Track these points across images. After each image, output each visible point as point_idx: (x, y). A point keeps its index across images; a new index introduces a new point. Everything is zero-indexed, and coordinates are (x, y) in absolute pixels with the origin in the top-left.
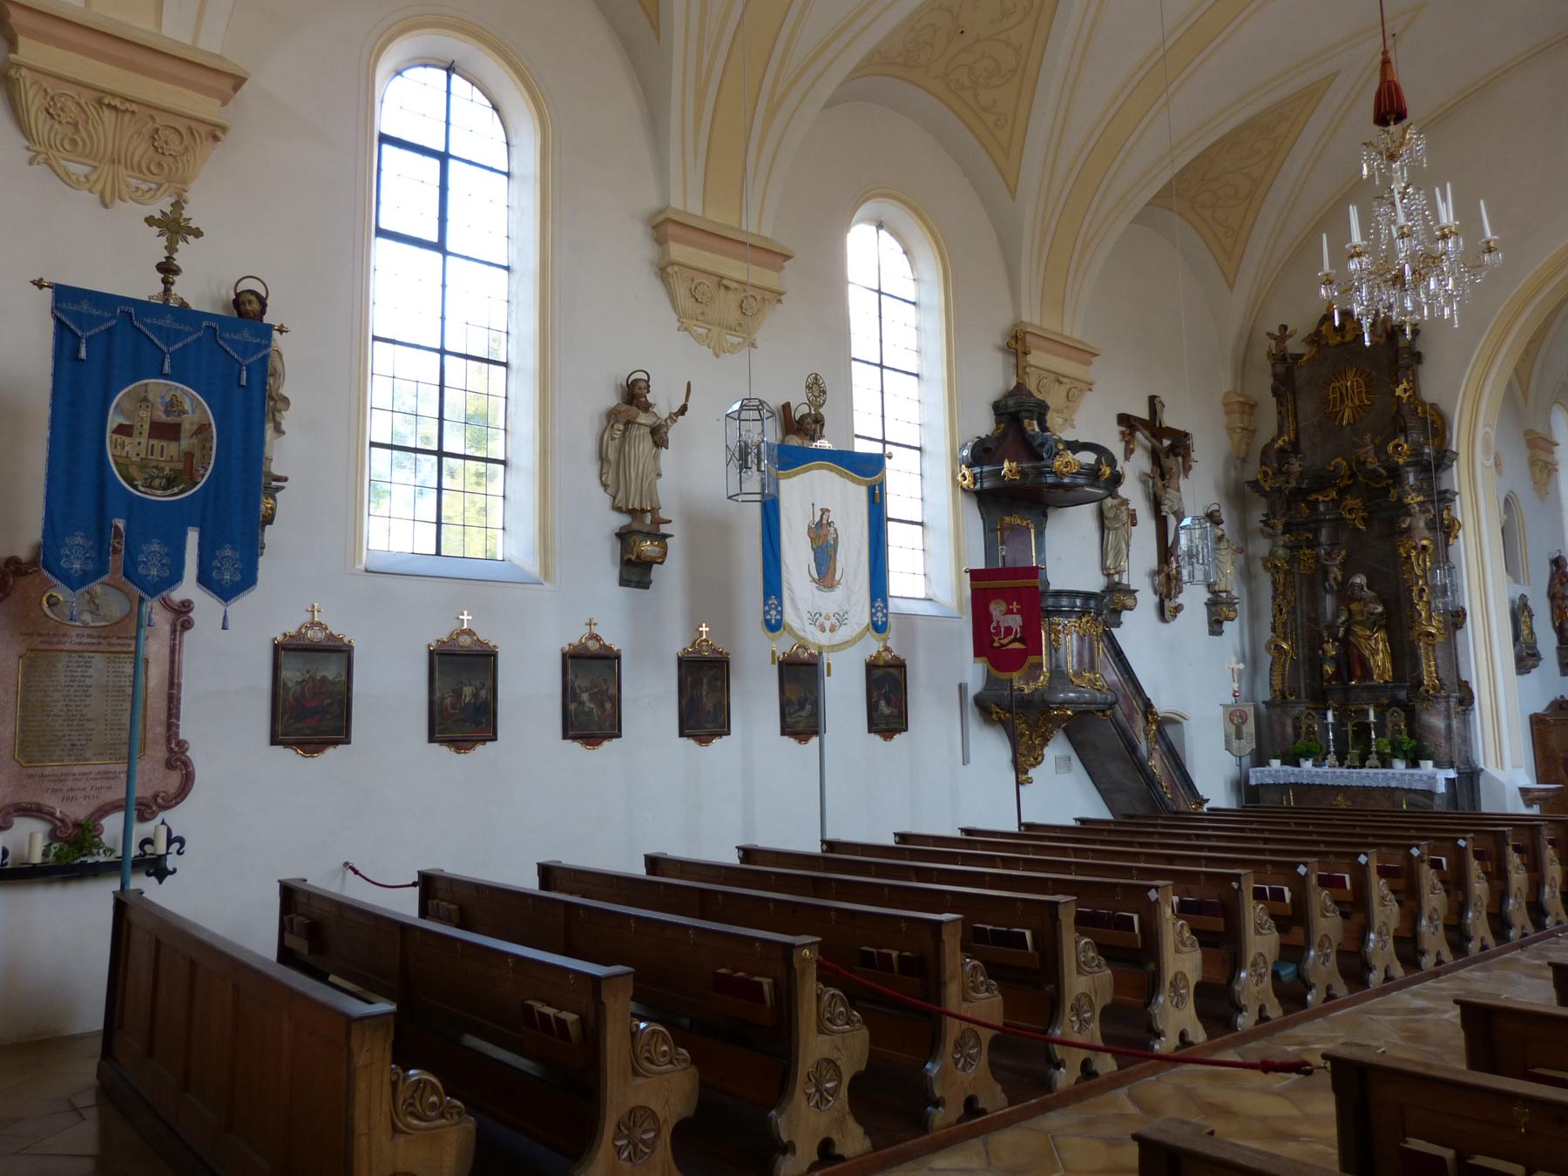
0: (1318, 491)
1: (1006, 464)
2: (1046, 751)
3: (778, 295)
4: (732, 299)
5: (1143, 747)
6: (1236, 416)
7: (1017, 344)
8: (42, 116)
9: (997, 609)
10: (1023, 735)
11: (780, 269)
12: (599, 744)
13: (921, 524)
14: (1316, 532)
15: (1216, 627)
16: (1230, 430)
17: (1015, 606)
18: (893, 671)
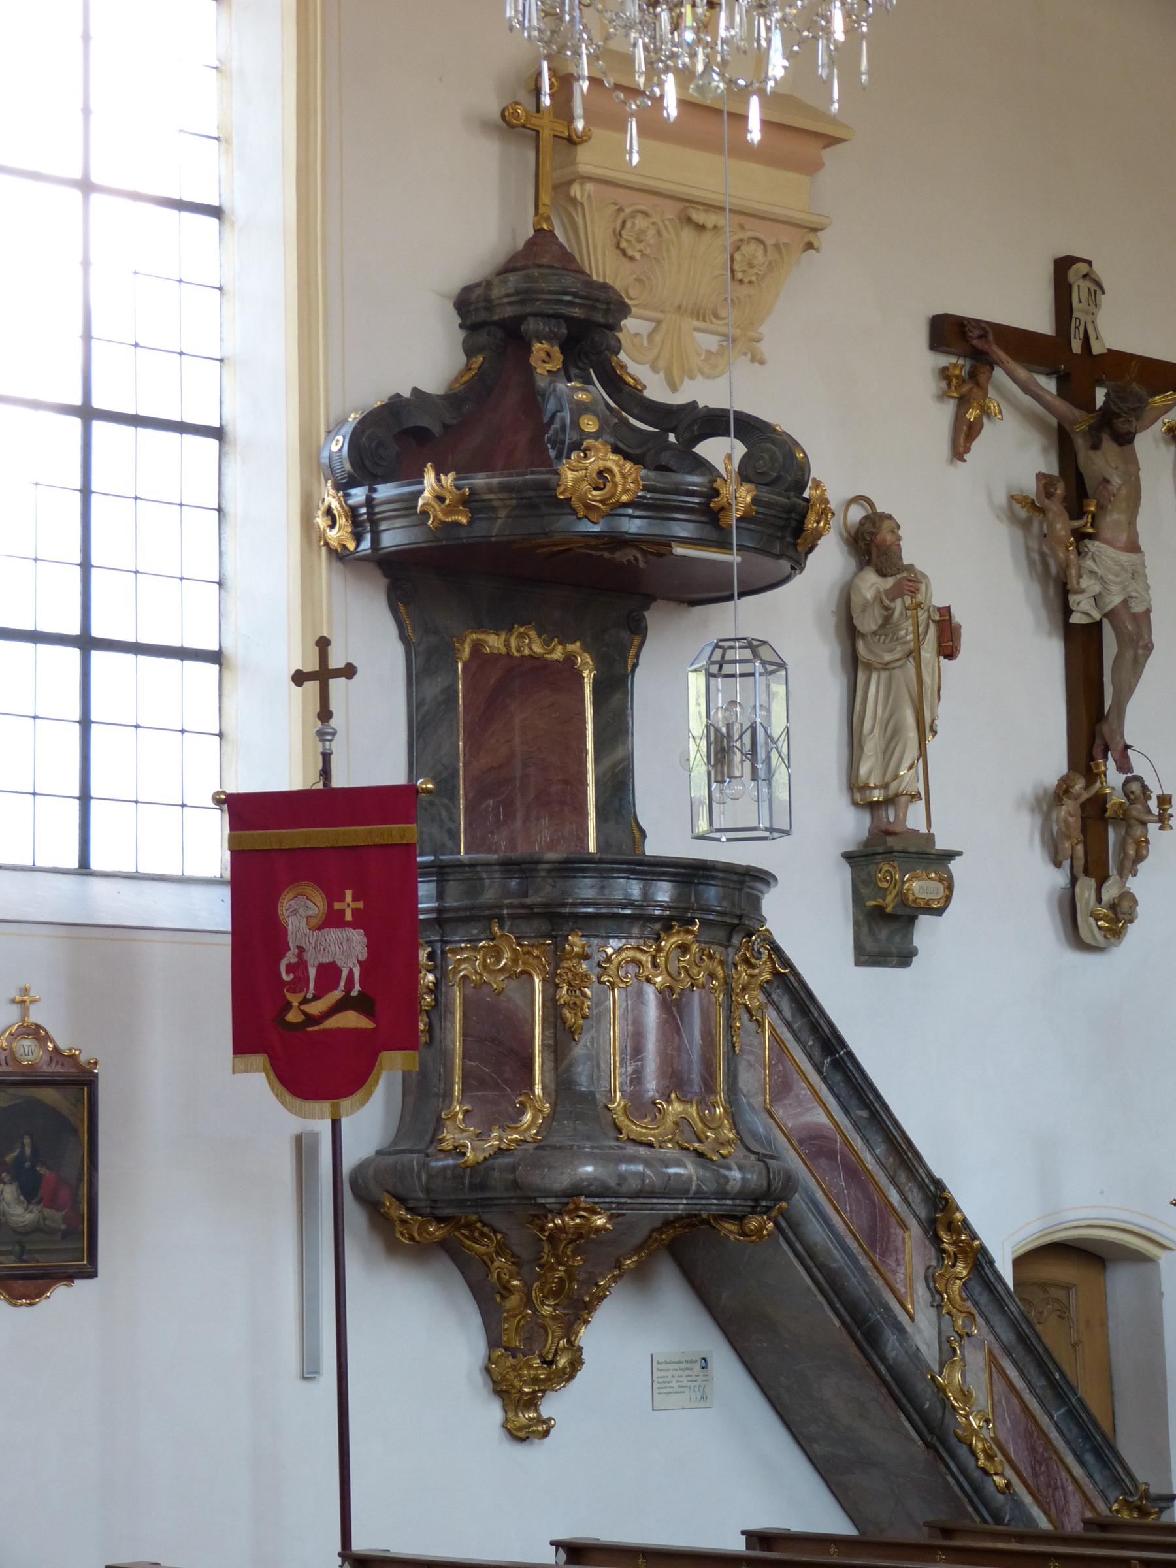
1: (429, 478)
2: (589, 1337)
3: (809, 235)
4: (710, 253)
5: (923, 1329)
7: (537, 127)
8: (611, 252)
9: (299, 911)
10: (506, 1290)
11: (811, 167)
12: (40, 1294)
13: (216, 657)
17: (349, 904)
18: (49, 1095)
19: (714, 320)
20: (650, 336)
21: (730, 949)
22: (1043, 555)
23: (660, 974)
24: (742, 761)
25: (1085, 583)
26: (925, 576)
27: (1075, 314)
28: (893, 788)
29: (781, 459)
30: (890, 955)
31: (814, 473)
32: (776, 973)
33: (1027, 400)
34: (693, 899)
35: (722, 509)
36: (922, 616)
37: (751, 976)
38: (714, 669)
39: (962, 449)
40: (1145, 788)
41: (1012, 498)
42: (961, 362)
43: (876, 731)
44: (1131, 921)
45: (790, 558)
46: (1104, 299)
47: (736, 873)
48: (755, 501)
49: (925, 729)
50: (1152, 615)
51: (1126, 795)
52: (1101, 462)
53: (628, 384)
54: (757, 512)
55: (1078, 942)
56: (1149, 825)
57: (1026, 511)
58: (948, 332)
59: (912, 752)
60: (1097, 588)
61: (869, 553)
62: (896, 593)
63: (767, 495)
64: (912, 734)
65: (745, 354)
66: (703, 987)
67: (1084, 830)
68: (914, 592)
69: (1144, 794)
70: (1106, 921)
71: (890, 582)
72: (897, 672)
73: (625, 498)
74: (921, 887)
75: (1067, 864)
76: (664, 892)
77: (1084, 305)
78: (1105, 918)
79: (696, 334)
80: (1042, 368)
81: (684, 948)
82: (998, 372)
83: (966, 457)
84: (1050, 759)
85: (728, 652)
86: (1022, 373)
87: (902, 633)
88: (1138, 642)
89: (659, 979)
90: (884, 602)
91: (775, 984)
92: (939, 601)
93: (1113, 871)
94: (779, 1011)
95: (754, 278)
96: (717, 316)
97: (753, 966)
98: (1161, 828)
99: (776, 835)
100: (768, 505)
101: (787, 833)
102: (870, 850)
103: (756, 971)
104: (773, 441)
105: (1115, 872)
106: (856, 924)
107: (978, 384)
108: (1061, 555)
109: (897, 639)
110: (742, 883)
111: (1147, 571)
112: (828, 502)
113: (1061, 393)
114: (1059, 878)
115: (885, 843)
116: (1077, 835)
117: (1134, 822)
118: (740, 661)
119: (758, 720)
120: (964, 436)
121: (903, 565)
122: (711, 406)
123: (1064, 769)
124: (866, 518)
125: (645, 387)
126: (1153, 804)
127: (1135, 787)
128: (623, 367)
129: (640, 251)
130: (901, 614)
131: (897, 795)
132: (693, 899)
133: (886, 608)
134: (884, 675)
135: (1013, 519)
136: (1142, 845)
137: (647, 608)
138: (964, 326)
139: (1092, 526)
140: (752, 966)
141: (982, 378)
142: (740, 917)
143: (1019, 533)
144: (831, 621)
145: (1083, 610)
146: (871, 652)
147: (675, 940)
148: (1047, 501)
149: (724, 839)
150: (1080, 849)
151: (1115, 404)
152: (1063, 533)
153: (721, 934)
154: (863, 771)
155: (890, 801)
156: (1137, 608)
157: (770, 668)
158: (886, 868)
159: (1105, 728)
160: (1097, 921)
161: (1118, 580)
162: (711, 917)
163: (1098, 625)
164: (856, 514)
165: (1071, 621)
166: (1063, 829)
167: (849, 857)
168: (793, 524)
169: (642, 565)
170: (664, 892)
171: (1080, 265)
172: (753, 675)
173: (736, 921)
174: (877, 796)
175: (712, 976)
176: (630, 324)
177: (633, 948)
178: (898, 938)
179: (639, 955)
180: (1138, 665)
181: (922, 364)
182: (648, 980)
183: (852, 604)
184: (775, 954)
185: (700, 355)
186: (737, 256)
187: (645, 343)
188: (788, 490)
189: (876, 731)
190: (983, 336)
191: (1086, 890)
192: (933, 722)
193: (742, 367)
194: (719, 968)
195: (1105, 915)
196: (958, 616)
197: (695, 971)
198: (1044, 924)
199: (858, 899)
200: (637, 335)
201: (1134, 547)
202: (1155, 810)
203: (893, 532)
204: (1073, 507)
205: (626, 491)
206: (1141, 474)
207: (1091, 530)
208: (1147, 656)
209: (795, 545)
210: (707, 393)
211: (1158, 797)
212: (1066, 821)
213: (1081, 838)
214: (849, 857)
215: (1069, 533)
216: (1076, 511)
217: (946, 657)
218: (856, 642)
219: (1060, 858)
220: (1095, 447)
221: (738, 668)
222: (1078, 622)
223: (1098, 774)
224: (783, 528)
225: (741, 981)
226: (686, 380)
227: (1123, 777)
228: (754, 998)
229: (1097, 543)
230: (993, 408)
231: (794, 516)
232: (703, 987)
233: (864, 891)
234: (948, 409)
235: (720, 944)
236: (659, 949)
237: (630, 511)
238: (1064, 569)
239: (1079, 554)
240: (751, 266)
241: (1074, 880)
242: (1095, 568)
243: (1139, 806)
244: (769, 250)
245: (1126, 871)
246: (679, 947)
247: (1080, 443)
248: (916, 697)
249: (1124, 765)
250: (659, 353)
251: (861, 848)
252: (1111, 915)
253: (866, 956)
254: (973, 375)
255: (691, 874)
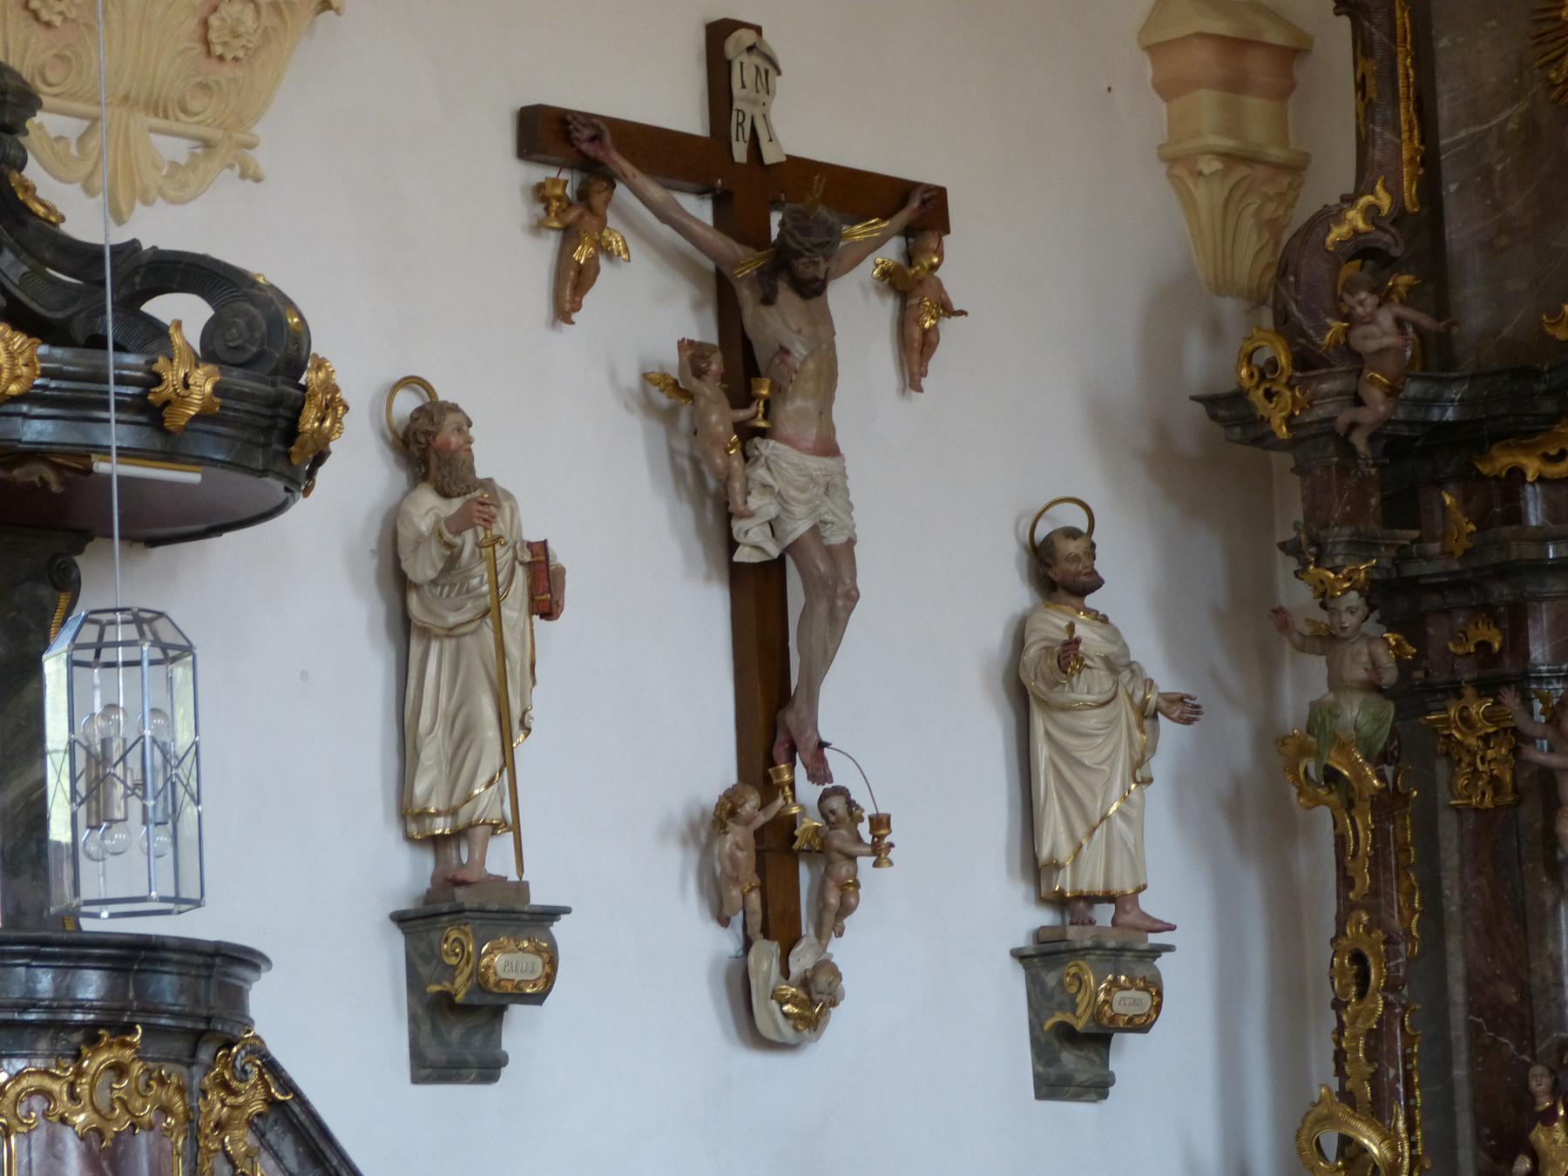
0: (1522, 434)
6: (1206, 102)
14: (1515, 622)
15: (1073, 1053)
16: (1177, 161)
19: (182, 116)
20: (82, 140)
21: (195, 1068)
22: (695, 462)
23: (83, 1110)
24: (126, 796)
25: (754, 502)
26: (509, 496)
27: (737, 105)
28: (464, 813)
29: (264, 326)
30: (465, 1065)
31: (318, 347)
32: (271, 1102)
33: (666, 231)
34: (131, 994)
35: (167, 403)
36: (503, 556)
37: (233, 1107)
38: (88, 655)
39: (568, 306)
40: (850, 804)
41: (646, 377)
42: (565, 175)
43: (439, 730)
44: (834, 1004)
45: (279, 476)
46: (779, 83)
47: (199, 953)
48: (217, 390)
49: (510, 726)
50: (856, 548)
51: (824, 816)
52: (776, 324)
53: (35, 215)
54: (222, 407)
55: (756, 1038)
56: (859, 860)
57: (669, 394)
58: (545, 132)
59: (491, 760)
60: (771, 510)
61: (426, 463)
62: (460, 523)
63: (240, 380)
64: (491, 733)
65: (231, 166)
66: (151, 1127)
67: (761, 869)
68: (489, 521)
69: (850, 813)
70: (796, 1005)
71: (457, 504)
72: (468, 640)
73: (14, 389)
74: (507, 963)
75: (737, 920)
76: (91, 985)
77: (750, 91)
78: (793, 1000)
79: (154, 137)
80: (688, 185)
81: (119, 1070)
82: (621, 190)
83: (575, 317)
84: (710, 762)
85: (109, 629)
86: (656, 192)
87: (475, 582)
88: (837, 592)
89: (80, 1119)
90: (446, 537)
91: (272, 1118)
92: (532, 534)
93: (807, 928)
94: (278, 1158)
95: (241, 54)
96: (185, 111)
97: (234, 1093)
98: (876, 865)
99: (183, 907)
100: (241, 396)
101: (197, 904)
102: (431, 909)
103: (241, 1099)
104: (252, 300)
105: (812, 932)
106: (413, 1020)
107: (591, 209)
108: (719, 461)
109: (468, 591)
110: (210, 967)
111: (849, 483)
112: (337, 390)
113: (722, 221)
114: (727, 942)
115: (452, 897)
116: (750, 877)
117: (836, 856)
118: (125, 644)
119: (148, 733)
120: (571, 287)
121: (477, 480)
122: (162, 247)
123: (732, 778)
124: (420, 410)
125: (63, 219)
126: (864, 829)
127: (836, 803)
128: (29, 188)
129: (61, 13)
130: (473, 553)
131: (472, 825)
132: (131, 994)
133: (449, 545)
134: (449, 645)
135: (649, 407)
136: (849, 888)
137: (80, 551)
138: (568, 123)
139: (765, 417)
140: (234, 1093)
141: (597, 200)
142: (208, 1020)
143: (659, 430)
144: (370, 565)
145: (755, 544)
146: (429, 611)
147: (105, 1057)
148: (695, 382)
149: (105, 914)
150: (755, 899)
151: (793, 237)
152: (721, 429)
153: (179, 1046)
154: (420, 788)
155: (459, 835)
156: (836, 538)
157: (172, 653)
158: (454, 935)
159: (790, 718)
160: (781, 1004)
161: (803, 497)
162: (163, 1021)
163: (781, 561)
164: (407, 403)
165: (736, 559)
166: (729, 869)
167: (401, 919)
168: (282, 424)
169: (55, 488)
170: (91, 985)
171: (742, 33)
172: (138, 663)
173: (202, 1026)
174: (441, 826)
175: (165, 1110)
176: (45, 124)
177: (38, 1072)
178: (477, 1040)
179: (47, 1083)
180: (837, 622)
181: (508, 180)
182: (63, 1120)
183: (400, 540)
184: (270, 1071)
185: (159, 168)
186: (214, 21)
187: (73, 151)
188: (275, 372)
189: (439, 730)
190: (596, 138)
191: (765, 958)
192: (524, 713)
193: (226, 187)
194: (177, 1098)
195: (794, 996)
196: (560, 554)
197: (138, 1103)
198: (702, 1011)
199: (415, 982)
200: (59, 139)
201: (829, 449)
202: (868, 838)
203: (459, 430)
204: (735, 393)
205: (15, 378)
206: (837, 339)
207: (762, 424)
208: (850, 610)
209: (288, 456)
210: (161, 229)
211: (871, 819)
212: (732, 857)
213: (756, 881)
214: (401, 919)
215: (730, 427)
216: (740, 396)
217: (543, 616)
218: (408, 597)
219: (727, 912)
220: (768, 300)
221: (121, 655)
222: (746, 560)
223: (781, 787)
224: (267, 430)
225: (214, 1116)
226: (138, 205)
227: (819, 790)
228: (240, 1141)
229: (772, 443)
230: (616, 245)
231: (282, 411)
232: (151, 1127)
233: (424, 970)
234: (547, 247)
235: (178, 1061)
236: (79, 1073)
237: (25, 408)
238: (725, 481)
239: (746, 458)
240: (237, 36)
241: (748, 944)
242: (770, 480)
243: (844, 832)
244: (264, 13)
245: (825, 930)
246: (111, 1067)
247: (746, 296)
248: (494, 675)
249: (819, 773)
250: (96, 165)
251: (420, 905)
252: (802, 995)
253: (429, 1067)
254: (583, 195)
255: (133, 957)
